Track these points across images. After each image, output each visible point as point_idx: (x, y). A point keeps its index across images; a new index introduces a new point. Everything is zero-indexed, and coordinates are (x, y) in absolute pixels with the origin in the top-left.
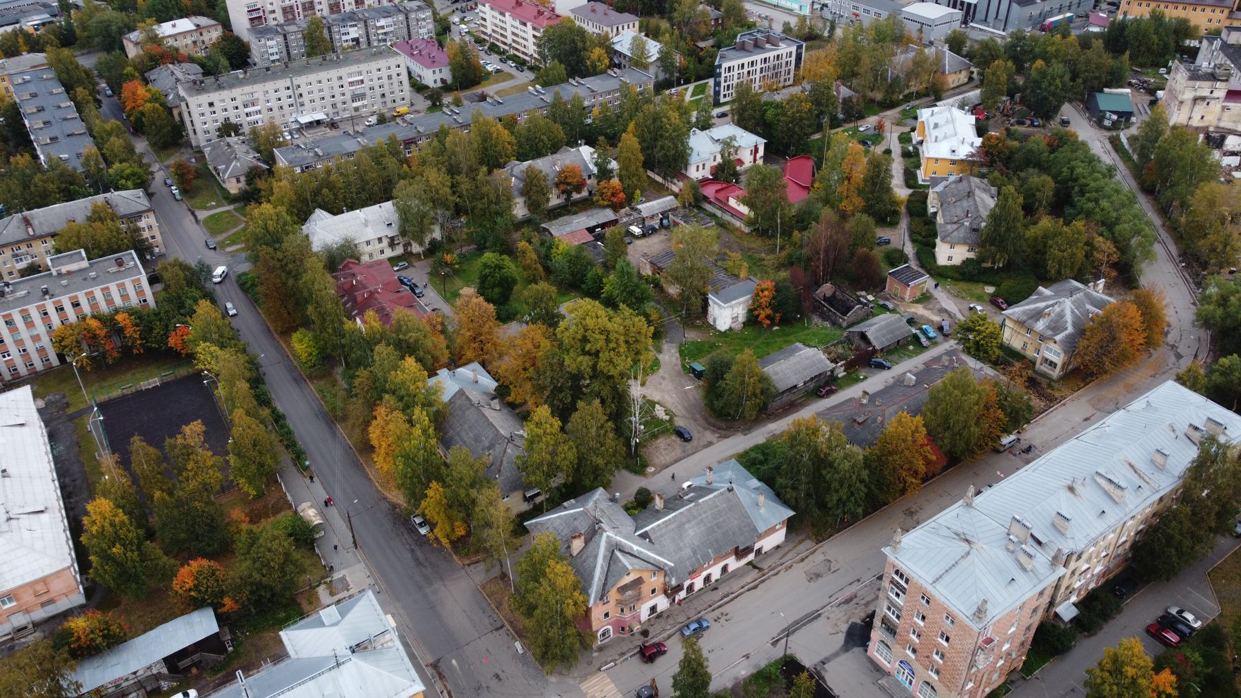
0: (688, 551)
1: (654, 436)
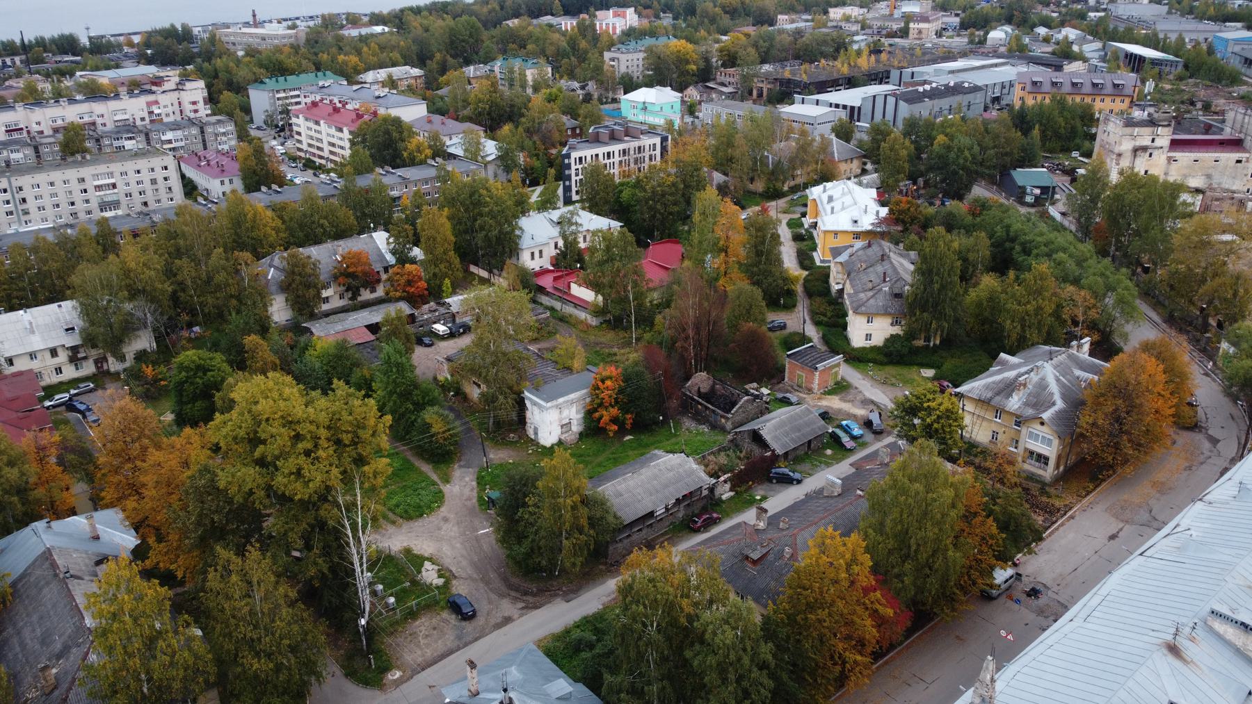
1: (412, 615)
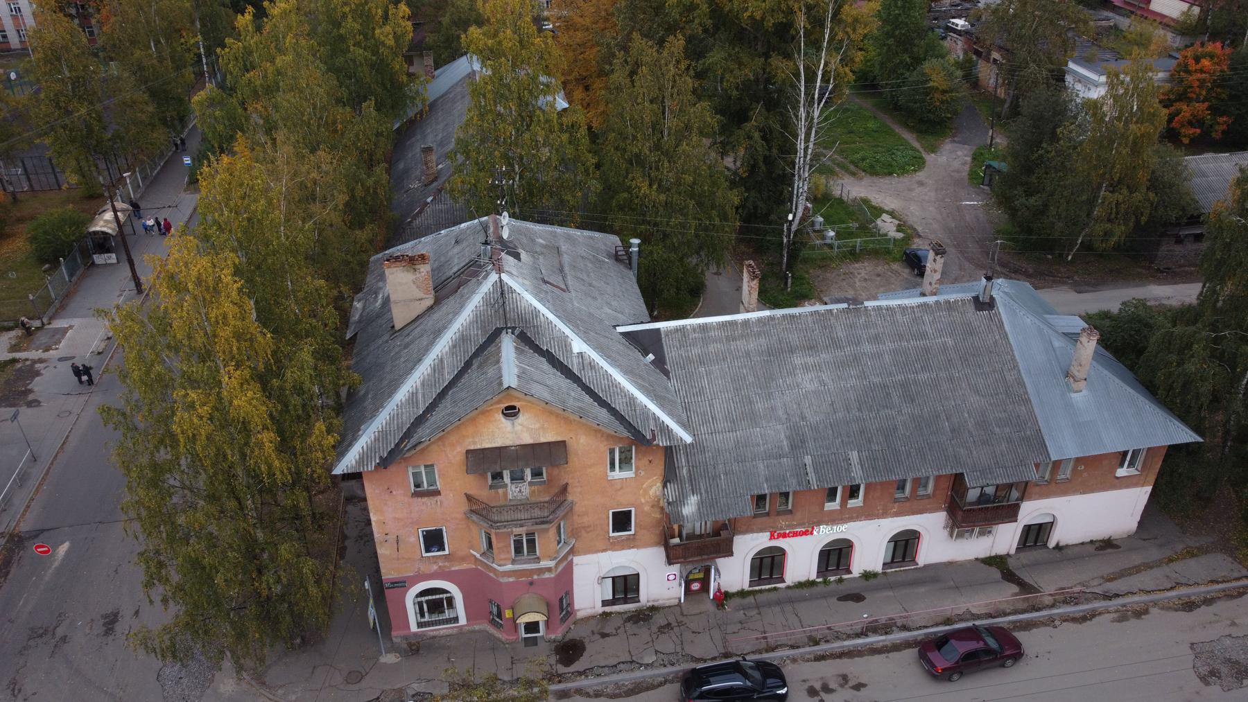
0: (776, 433)
1: (854, 255)
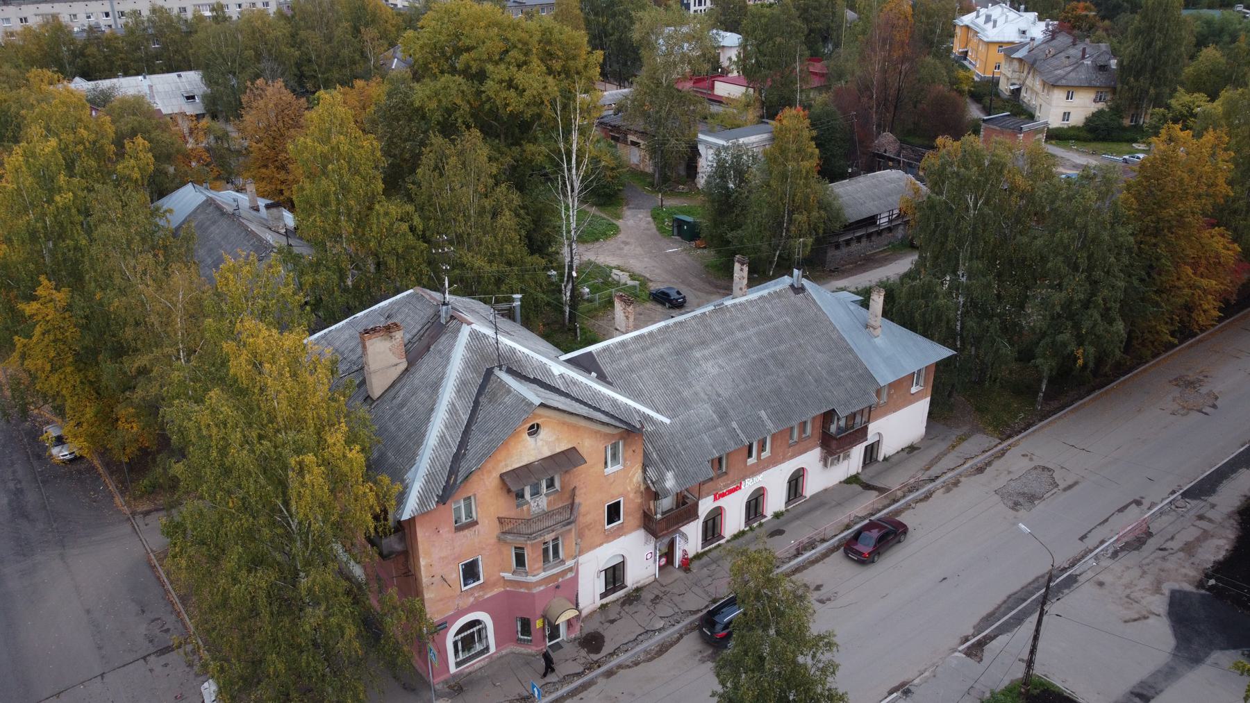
0: (705, 411)
